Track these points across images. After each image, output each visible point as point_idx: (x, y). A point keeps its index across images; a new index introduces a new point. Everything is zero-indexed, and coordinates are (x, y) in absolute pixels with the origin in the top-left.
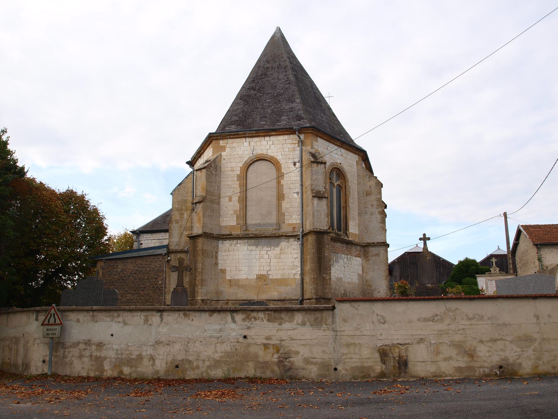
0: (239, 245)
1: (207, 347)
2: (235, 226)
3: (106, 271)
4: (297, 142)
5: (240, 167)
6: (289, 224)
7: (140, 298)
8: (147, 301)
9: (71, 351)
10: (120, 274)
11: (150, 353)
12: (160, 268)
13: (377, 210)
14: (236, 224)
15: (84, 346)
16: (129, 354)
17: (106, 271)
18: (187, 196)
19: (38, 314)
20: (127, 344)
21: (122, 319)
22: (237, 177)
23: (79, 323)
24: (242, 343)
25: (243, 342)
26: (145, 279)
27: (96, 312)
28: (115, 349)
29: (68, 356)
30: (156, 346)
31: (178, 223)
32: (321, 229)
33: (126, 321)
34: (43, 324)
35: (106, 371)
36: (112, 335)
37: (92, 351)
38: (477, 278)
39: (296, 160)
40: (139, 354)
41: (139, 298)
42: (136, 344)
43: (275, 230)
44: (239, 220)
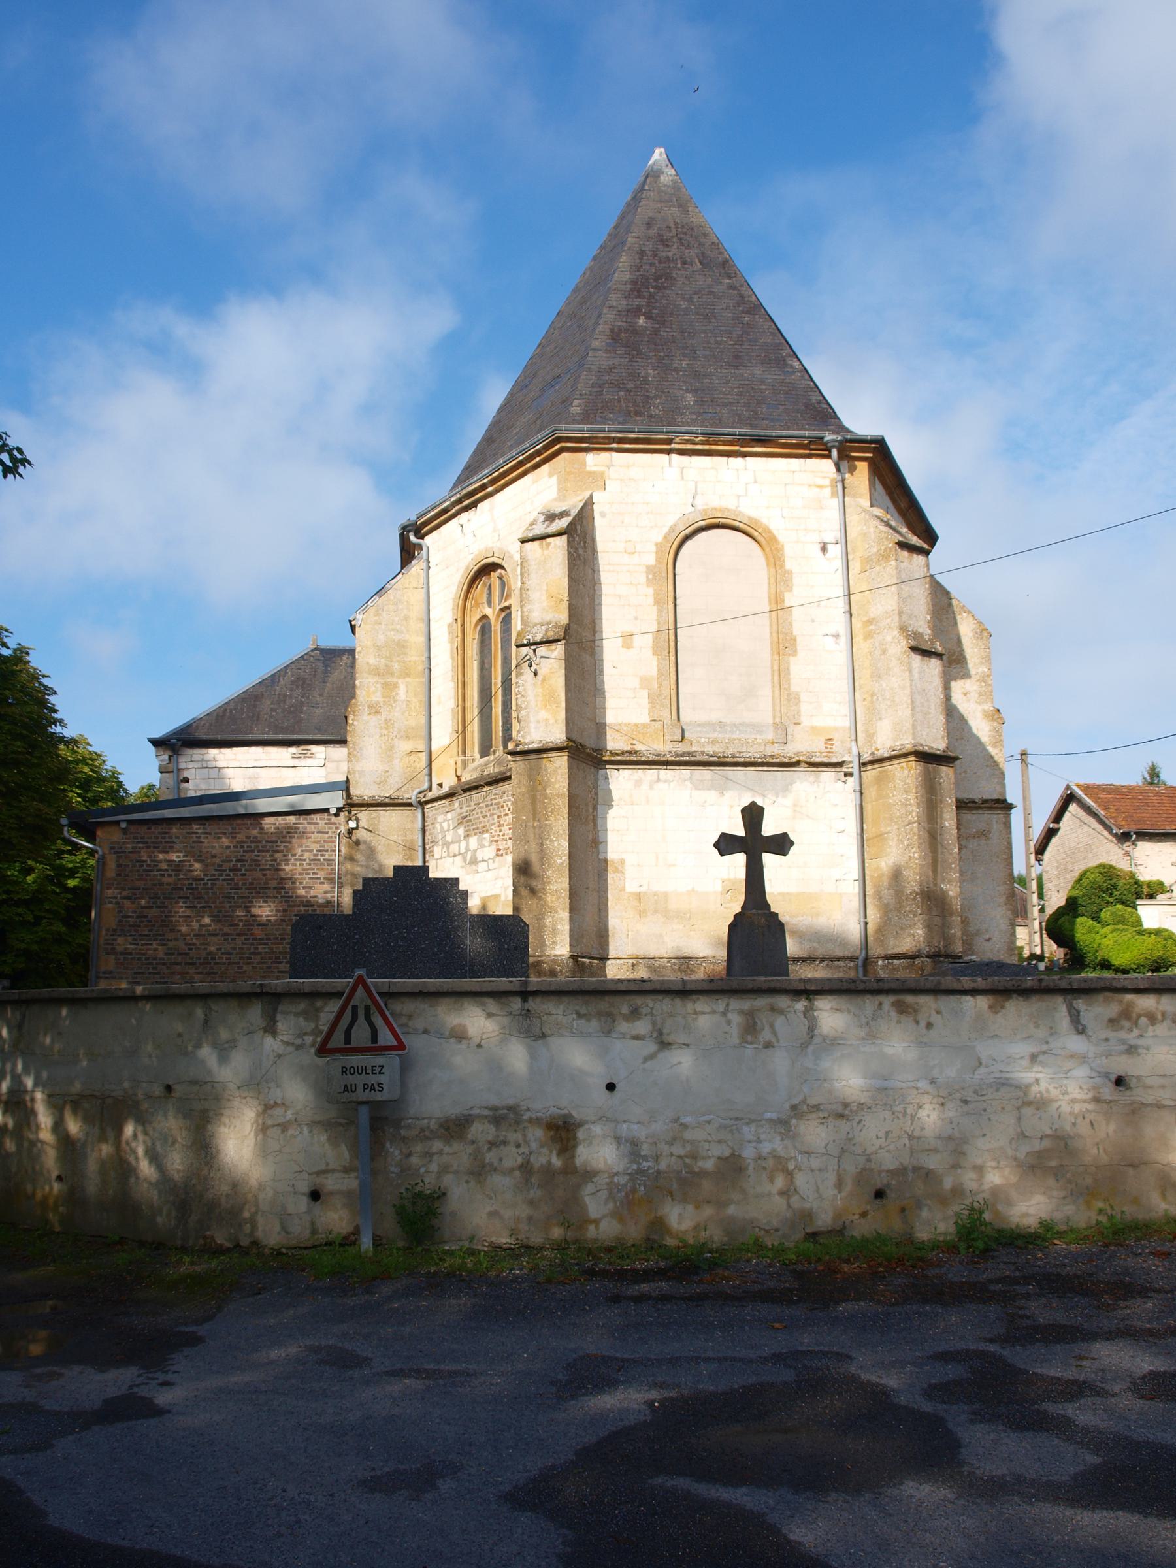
0: (661, 785)
1: (990, 1119)
2: (645, 726)
3: (132, 861)
4: (827, 482)
5: (656, 544)
6: (814, 730)
7: (252, 950)
8: (279, 958)
9: (434, 1149)
10: (180, 870)
11: (774, 1150)
12: (322, 855)
13: (980, 708)
14: (648, 721)
15: (492, 1129)
16: (687, 1157)
17: (132, 861)
18: (408, 631)
19: (275, 1010)
20: (678, 1118)
21: (650, 1027)
22: (647, 574)
23: (464, 1042)
24: (1111, 1101)
25: (1116, 1098)
26: (269, 888)
27: (538, 999)
28: (626, 1141)
29: (422, 1170)
30: (794, 1121)
31: (377, 712)
32: (932, 748)
33: (668, 1034)
34: (322, 1050)
35: (596, 1222)
36: (611, 1087)
37: (526, 1151)
38: (1139, 907)
39: (829, 537)
40: (727, 1153)
41: (250, 949)
42: (712, 1116)
43: (773, 743)
44: (658, 707)
